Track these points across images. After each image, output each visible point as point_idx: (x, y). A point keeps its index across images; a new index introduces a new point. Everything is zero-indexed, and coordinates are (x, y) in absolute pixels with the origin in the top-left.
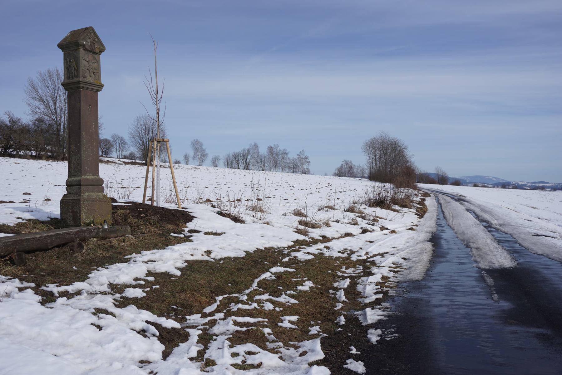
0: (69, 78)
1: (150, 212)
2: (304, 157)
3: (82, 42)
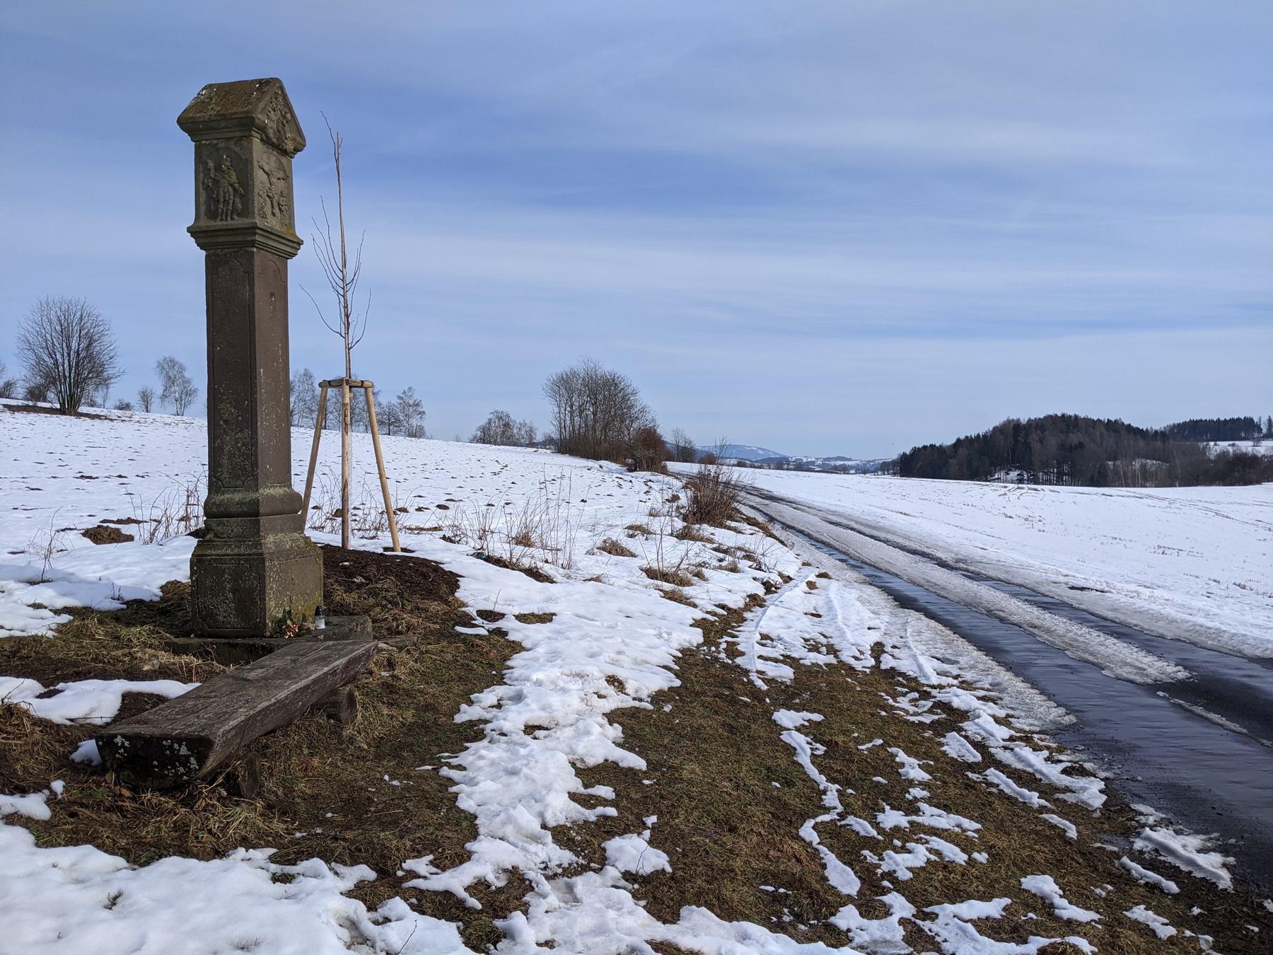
0: (212, 214)
1: (372, 570)
2: (411, 402)
3: (261, 117)
